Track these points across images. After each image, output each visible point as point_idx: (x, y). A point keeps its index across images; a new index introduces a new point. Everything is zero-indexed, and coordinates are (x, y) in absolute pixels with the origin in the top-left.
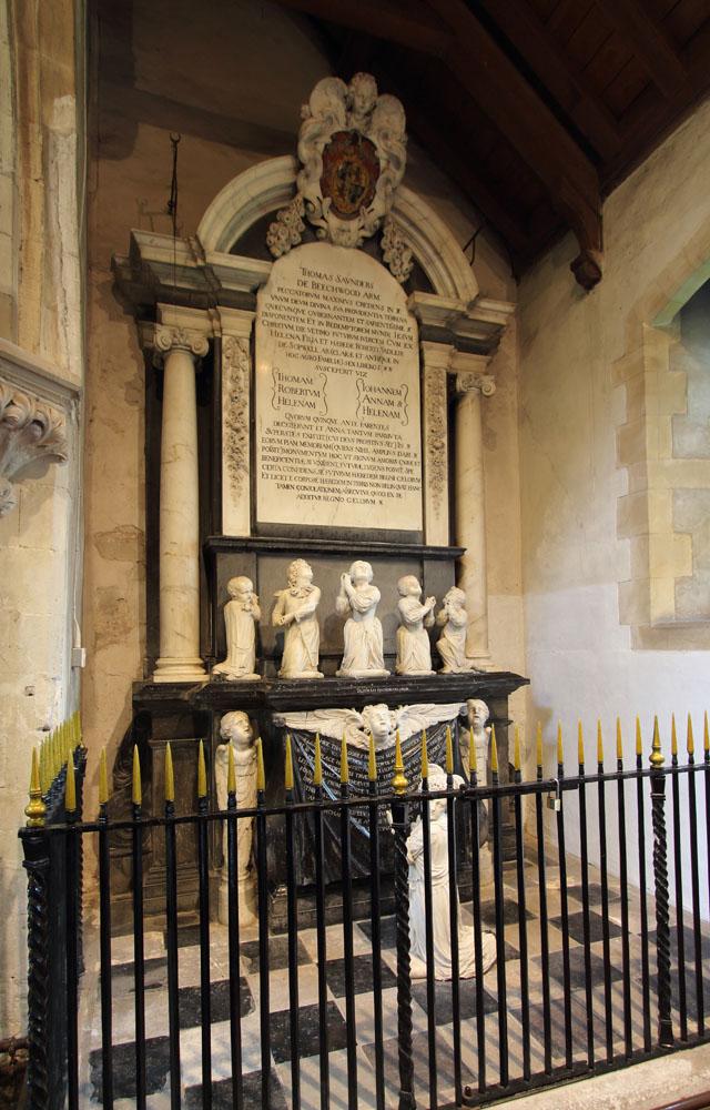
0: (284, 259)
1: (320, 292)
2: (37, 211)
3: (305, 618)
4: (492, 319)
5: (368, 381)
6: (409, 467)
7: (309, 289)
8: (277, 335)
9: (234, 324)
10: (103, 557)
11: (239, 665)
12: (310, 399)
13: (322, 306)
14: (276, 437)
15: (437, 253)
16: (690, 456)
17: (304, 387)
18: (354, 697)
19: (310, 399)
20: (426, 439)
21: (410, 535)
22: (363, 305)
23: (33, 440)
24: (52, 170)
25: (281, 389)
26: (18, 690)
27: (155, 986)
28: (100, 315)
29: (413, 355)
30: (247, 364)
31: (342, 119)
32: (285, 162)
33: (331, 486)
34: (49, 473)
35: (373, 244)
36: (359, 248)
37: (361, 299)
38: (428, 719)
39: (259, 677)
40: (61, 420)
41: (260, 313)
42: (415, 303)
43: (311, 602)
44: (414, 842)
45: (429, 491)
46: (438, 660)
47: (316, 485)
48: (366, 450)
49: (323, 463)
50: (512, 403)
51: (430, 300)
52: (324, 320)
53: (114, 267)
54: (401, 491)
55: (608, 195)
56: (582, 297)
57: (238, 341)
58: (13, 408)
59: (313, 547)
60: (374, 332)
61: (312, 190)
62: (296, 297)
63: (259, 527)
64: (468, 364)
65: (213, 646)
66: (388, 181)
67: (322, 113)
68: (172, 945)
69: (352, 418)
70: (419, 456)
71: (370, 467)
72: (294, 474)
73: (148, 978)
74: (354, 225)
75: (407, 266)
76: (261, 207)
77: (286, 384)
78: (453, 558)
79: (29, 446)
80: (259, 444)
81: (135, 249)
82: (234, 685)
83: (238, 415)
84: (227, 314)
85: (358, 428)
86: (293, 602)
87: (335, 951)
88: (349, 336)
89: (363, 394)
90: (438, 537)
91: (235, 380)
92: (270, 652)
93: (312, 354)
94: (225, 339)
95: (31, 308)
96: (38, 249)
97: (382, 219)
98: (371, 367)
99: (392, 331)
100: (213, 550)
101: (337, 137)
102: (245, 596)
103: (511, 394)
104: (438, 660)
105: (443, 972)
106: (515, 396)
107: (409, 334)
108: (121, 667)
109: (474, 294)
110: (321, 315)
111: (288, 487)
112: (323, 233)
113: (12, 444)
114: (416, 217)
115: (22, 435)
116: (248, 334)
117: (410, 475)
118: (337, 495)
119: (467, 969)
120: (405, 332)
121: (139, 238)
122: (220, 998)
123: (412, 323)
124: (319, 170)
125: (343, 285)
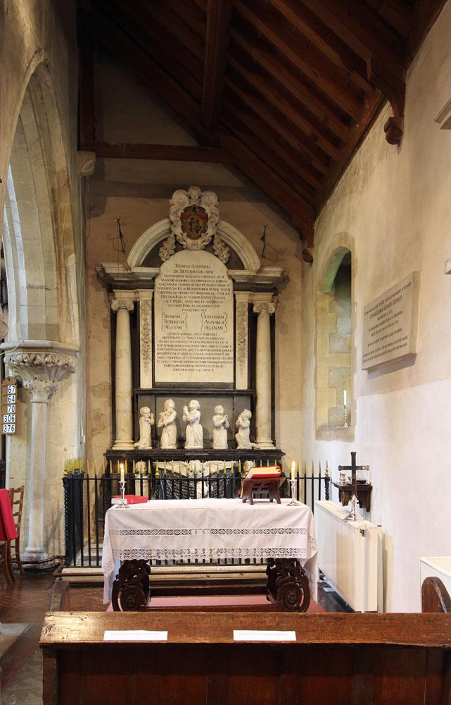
1: (184, 274)
2: (64, 294)
3: (169, 424)
4: (273, 275)
5: (207, 313)
7: (179, 274)
8: (164, 297)
9: (145, 295)
11: (145, 443)
12: (179, 325)
13: (185, 280)
16: (337, 352)
18: (181, 454)
19: (179, 325)
22: (205, 277)
26: (62, 450)
28: (92, 289)
30: (150, 312)
31: (188, 202)
32: (166, 221)
33: (189, 364)
34: (70, 378)
35: (209, 247)
37: (204, 274)
40: (72, 361)
41: (156, 288)
43: (172, 418)
49: (186, 354)
50: (298, 308)
52: (186, 287)
57: (146, 302)
61: (178, 231)
65: (136, 436)
67: (178, 202)
69: (199, 331)
71: (207, 354)
74: (199, 241)
77: (167, 319)
78: (251, 396)
81: (103, 270)
82: (141, 451)
85: (202, 336)
86: (165, 417)
88: (198, 293)
92: (156, 435)
95: (63, 325)
96: (65, 305)
97: (213, 237)
98: (209, 306)
99: (219, 288)
100: (137, 395)
101: (186, 210)
103: (298, 303)
106: (299, 305)
108: (101, 443)
110: (184, 285)
111: (169, 366)
114: (229, 233)
116: (151, 299)
117: (228, 356)
118: (191, 368)
120: (226, 287)
121: (104, 266)
123: (230, 282)
124: (180, 223)
125: (195, 269)
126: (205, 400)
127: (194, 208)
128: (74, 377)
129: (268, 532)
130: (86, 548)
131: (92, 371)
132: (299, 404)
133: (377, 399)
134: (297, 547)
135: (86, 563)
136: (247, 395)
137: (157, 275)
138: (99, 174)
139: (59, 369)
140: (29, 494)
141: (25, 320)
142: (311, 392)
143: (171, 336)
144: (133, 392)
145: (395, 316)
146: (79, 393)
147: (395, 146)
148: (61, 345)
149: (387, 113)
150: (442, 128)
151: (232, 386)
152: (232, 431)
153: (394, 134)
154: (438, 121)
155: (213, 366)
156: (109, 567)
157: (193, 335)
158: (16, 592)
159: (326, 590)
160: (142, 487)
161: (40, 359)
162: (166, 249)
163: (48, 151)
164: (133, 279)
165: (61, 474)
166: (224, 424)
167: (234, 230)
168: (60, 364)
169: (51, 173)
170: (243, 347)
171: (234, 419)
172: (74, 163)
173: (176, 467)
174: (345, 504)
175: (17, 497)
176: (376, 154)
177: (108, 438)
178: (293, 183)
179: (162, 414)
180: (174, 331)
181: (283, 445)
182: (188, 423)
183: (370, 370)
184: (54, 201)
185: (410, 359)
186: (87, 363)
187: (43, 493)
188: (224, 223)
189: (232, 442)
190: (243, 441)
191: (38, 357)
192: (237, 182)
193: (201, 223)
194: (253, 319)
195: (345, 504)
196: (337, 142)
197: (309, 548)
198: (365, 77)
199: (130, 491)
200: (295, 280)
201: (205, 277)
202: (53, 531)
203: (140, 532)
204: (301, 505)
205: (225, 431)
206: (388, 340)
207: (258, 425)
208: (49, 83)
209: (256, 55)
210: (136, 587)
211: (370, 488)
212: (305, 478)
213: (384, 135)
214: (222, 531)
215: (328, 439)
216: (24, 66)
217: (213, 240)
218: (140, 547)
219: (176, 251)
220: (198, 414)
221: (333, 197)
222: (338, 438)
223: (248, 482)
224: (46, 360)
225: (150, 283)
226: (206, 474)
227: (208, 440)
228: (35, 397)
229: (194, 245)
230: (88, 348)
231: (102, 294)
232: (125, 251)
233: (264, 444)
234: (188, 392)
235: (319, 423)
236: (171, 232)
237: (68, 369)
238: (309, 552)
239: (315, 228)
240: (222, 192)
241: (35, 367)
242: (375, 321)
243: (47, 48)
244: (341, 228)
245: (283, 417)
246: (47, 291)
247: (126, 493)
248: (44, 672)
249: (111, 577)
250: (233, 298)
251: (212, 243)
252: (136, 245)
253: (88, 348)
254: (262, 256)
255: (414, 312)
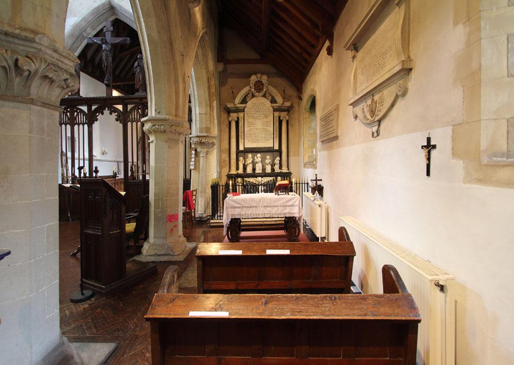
3: (250, 163)
9: (241, 115)
11: (241, 171)
18: (254, 175)
28: (222, 113)
32: (249, 86)
35: (264, 96)
40: (215, 141)
43: (251, 161)
78: (280, 151)
91: (241, 124)
95: (212, 128)
96: (212, 120)
100: (238, 152)
101: (256, 82)
108: (225, 171)
123: (272, 108)
126: (263, 154)
128: (215, 147)
129: (284, 206)
130: (219, 212)
131: (222, 144)
132: (298, 154)
133: (325, 153)
134: (295, 212)
135: (219, 218)
137: (245, 107)
138: (225, 70)
140: (199, 192)
141: (198, 126)
142: (302, 149)
144: (237, 151)
145: (331, 121)
146: (217, 152)
147: (330, 56)
148: (211, 135)
149: (327, 44)
150: (347, 50)
152: (273, 165)
153: (330, 52)
154: (345, 47)
156: (225, 221)
157: (258, 130)
158: (194, 229)
159: (307, 227)
160: (239, 189)
161: (203, 141)
163: (207, 64)
165: (210, 184)
167: (273, 89)
169: (208, 72)
170: (277, 133)
172: (216, 67)
173: (252, 180)
174: (313, 194)
175: (194, 193)
176: (324, 59)
177: (228, 169)
178: (295, 72)
179: (247, 160)
181: (292, 170)
182: (257, 163)
183: (322, 142)
184: (208, 82)
185: (336, 138)
186: (220, 141)
187: (204, 191)
189: (273, 170)
190: (277, 169)
192: (274, 71)
194: (280, 122)
195: (313, 194)
196: (310, 55)
197: (300, 212)
198: (319, 30)
199: (235, 191)
200: (296, 106)
202: (208, 206)
203: (237, 208)
204: (297, 195)
206: (329, 130)
207: (282, 163)
208: (207, 39)
209: (280, 24)
210: (236, 226)
211: (323, 188)
212: (297, 184)
213: (326, 52)
214: (267, 206)
215: (308, 168)
216: (198, 34)
218: (237, 213)
219: (252, 98)
220: (260, 159)
221: (309, 75)
222: (311, 167)
223: (277, 187)
226: (263, 182)
227: (264, 169)
228: (201, 155)
230: (221, 135)
231: (226, 115)
232: (234, 99)
233: (285, 170)
235: (305, 161)
236: (250, 90)
237: (213, 144)
238: (299, 214)
240: (269, 75)
241: (201, 144)
242: (324, 123)
243: (206, 27)
244: (312, 87)
245: (291, 159)
247: (233, 191)
248: (198, 266)
249: (226, 225)
251: (265, 94)
252: (238, 96)
253: (221, 135)
254: (284, 98)
255: (338, 120)
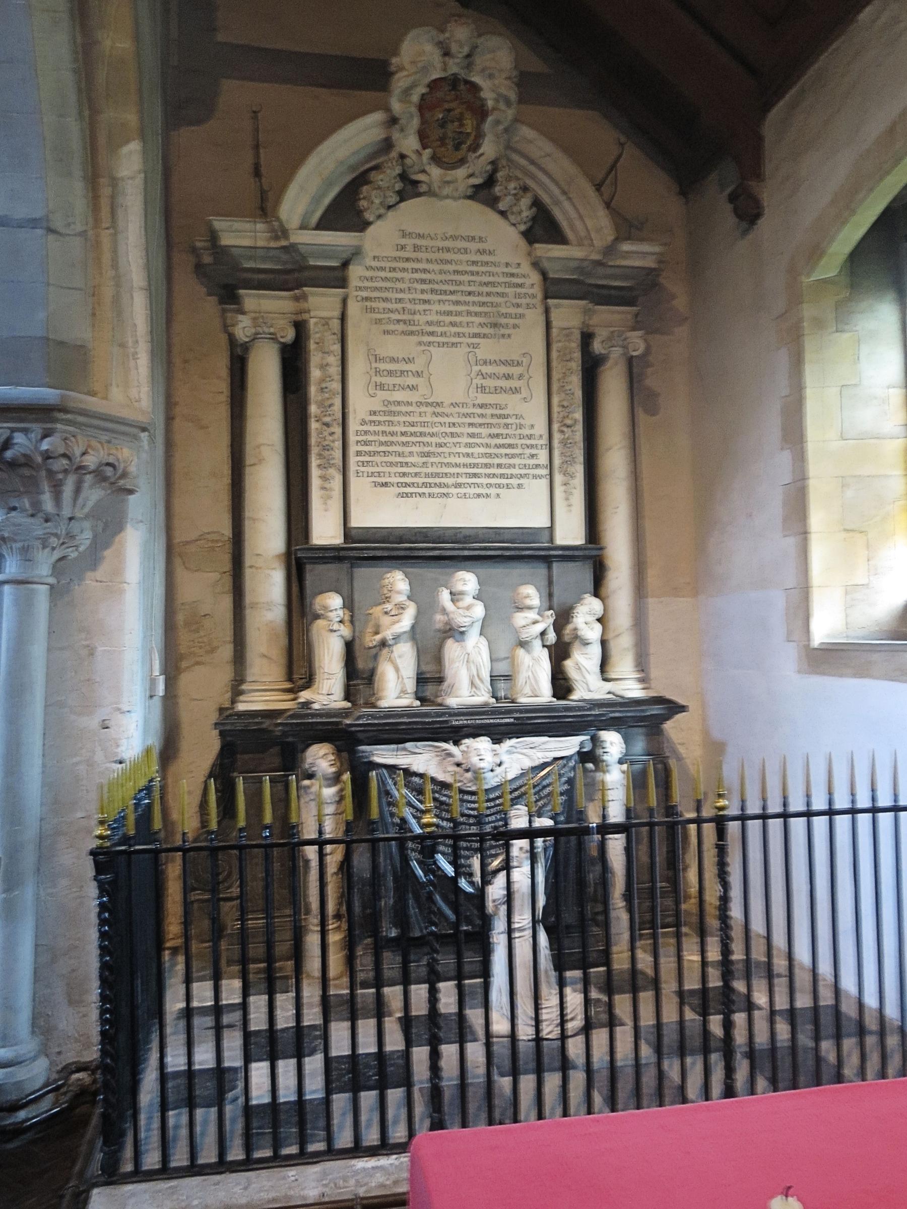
0: (379, 223)
2: (106, 258)
3: (397, 638)
4: (637, 263)
5: (481, 354)
6: (534, 451)
8: (373, 310)
9: (321, 304)
10: (186, 568)
11: (328, 692)
12: (411, 381)
14: (372, 428)
15: (564, 193)
17: (406, 367)
18: (448, 729)
19: (411, 381)
20: (555, 416)
21: (532, 533)
22: (474, 263)
23: (105, 479)
24: (120, 213)
25: (377, 372)
27: (230, 1026)
29: (535, 317)
30: (337, 348)
31: (439, 65)
32: (377, 117)
35: (484, 192)
36: (470, 197)
38: (540, 755)
39: (349, 705)
42: (536, 257)
43: (406, 622)
44: (496, 890)
45: (558, 478)
46: (561, 685)
47: (420, 480)
48: (478, 436)
49: (428, 455)
51: (557, 251)
53: (194, 250)
54: (521, 481)
55: (769, 111)
56: (745, 232)
57: (326, 322)
58: (86, 457)
59: (416, 553)
60: (488, 294)
61: (409, 143)
62: (394, 264)
63: (353, 532)
64: (608, 319)
65: (637, 833)
66: (498, 122)
68: (246, 992)
69: (460, 398)
70: (546, 436)
72: (394, 470)
73: (226, 1019)
74: (460, 173)
75: (527, 214)
76: (352, 168)
77: (382, 366)
78: (592, 560)
79: (103, 484)
80: (352, 438)
81: (213, 236)
83: (325, 406)
84: (313, 294)
86: (385, 620)
87: (420, 1007)
89: (476, 368)
90: (570, 532)
92: (359, 676)
93: (414, 328)
94: (312, 321)
96: (108, 292)
98: (485, 336)
100: (301, 560)
101: (434, 85)
102: (332, 615)
104: (561, 685)
105: (525, 1032)
107: (531, 291)
108: (206, 688)
109: (610, 238)
112: (423, 188)
113: (86, 485)
114: (535, 153)
115: (96, 476)
116: (337, 313)
119: (550, 1030)
122: (286, 1042)
123: (535, 278)
124: (416, 122)
127: (454, 82)
136: (585, 558)
137: (357, 253)
139: (89, 478)
143: (390, 409)
148: (93, 403)
151: (546, 536)
155: (499, 486)
162: (379, 188)
164: (289, 266)
165: (93, 835)
166: (543, 634)
168: (91, 461)
171: (563, 618)
177: (225, 675)
180: (399, 396)
188: (526, 132)
191: (19, 438)
193: (469, 125)
194: (591, 369)
201: (474, 263)
205: (545, 652)
217: (495, 171)
219: (403, 196)
220: (479, 610)
224: (45, 446)
225: (337, 274)
229: (448, 182)
231: (210, 305)
234: (436, 553)
239: (769, 130)
246: (51, 237)
250: (542, 318)
251: (490, 181)
